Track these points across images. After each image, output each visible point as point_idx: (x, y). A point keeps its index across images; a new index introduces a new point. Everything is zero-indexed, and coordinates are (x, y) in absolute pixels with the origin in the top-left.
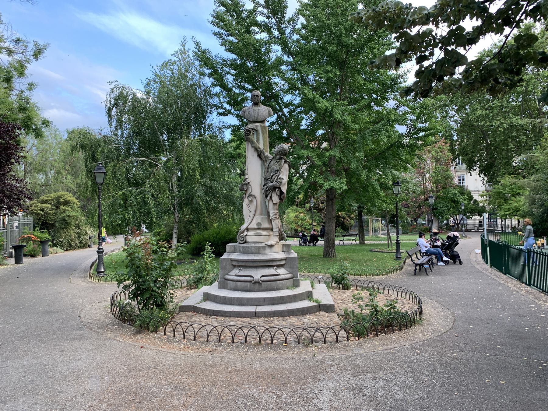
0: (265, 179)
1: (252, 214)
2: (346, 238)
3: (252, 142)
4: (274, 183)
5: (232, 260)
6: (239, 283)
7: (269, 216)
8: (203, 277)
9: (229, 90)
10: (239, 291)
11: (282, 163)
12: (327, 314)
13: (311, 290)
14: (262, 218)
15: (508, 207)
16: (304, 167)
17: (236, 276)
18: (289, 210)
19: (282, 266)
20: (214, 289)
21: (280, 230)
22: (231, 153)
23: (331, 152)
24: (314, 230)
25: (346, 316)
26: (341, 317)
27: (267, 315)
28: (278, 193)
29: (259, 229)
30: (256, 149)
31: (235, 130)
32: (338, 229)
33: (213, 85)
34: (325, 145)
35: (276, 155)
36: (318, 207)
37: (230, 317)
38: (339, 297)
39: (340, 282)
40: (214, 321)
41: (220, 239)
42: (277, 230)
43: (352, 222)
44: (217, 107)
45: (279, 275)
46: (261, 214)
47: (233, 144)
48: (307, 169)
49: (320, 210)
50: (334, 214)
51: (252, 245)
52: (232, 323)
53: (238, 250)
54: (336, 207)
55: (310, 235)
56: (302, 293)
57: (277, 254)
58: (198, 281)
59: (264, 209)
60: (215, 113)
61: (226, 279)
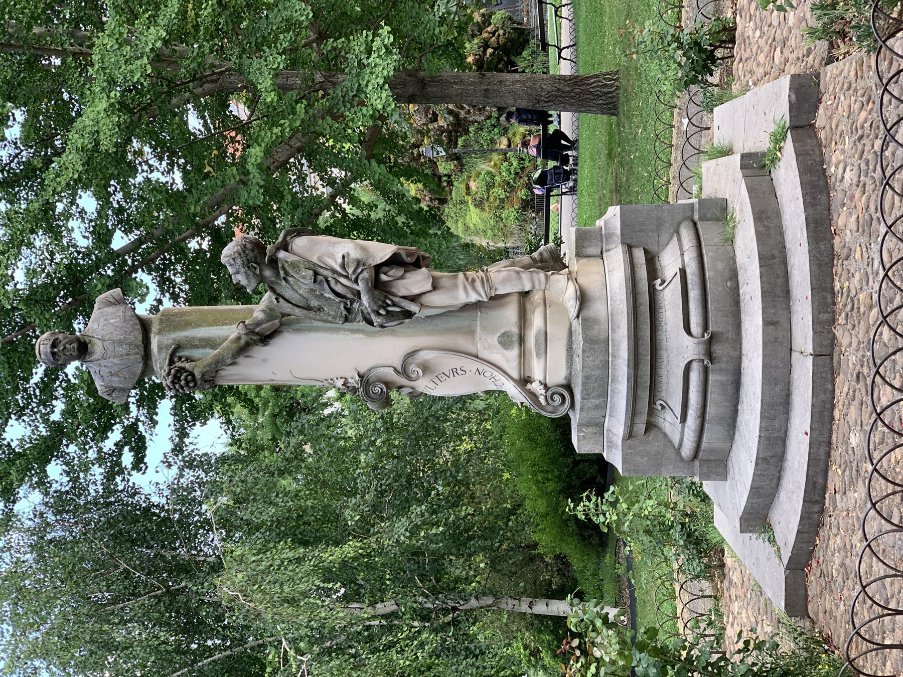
0: (346, 320)
1: (471, 365)
2: (551, 39)
3: (218, 365)
4: (361, 287)
5: (630, 435)
6: (711, 410)
7: (478, 305)
8: (683, 525)
9: (58, 432)
10: (735, 412)
11: (291, 258)
12: (827, 101)
13: (736, 159)
14: (484, 328)
16: (313, 179)
17: (684, 419)
18: (457, 229)
19: (651, 260)
20: (728, 501)
21: (526, 267)
22: (274, 416)
23: (265, 83)
24: (525, 144)
25: (834, 33)
26: (835, 52)
27: (826, 317)
28: (396, 272)
29: (522, 340)
30: (243, 349)
31: (189, 414)
32: (521, 65)
33: (43, 484)
34: (239, 109)
35: (261, 279)
36: (450, 132)
37: (829, 443)
38: (761, 58)
39: (708, 57)
40: (847, 500)
41: (553, 461)
42: (525, 276)
43: (498, 16)
44: (114, 470)
45: (683, 272)
46: (471, 332)
47: (239, 411)
48: (320, 169)
49: (459, 126)
50: (471, 76)
52: (855, 440)
53: (596, 414)
54: (448, 71)
55: (539, 160)
56: (750, 190)
57: (611, 276)
58: (697, 543)
59: (453, 322)
60: (136, 478)
61: (695, 456)
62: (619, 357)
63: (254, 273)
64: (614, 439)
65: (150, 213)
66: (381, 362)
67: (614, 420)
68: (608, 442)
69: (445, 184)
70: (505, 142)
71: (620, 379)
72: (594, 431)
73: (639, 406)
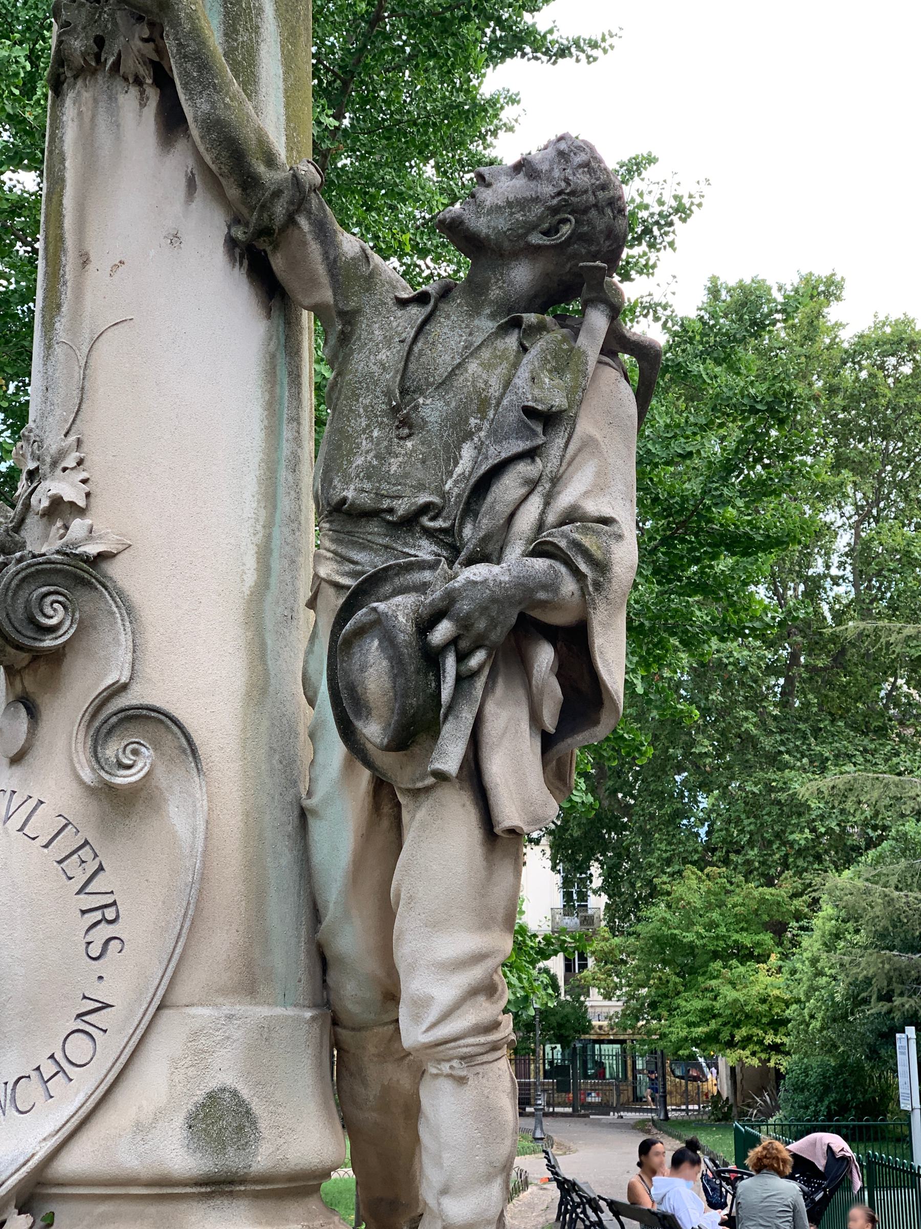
14: (265, 1033)
15: (698, 1004)
46: (249, 983)
63: (531, 227)
65: (411, 57)
66: (153, 638)
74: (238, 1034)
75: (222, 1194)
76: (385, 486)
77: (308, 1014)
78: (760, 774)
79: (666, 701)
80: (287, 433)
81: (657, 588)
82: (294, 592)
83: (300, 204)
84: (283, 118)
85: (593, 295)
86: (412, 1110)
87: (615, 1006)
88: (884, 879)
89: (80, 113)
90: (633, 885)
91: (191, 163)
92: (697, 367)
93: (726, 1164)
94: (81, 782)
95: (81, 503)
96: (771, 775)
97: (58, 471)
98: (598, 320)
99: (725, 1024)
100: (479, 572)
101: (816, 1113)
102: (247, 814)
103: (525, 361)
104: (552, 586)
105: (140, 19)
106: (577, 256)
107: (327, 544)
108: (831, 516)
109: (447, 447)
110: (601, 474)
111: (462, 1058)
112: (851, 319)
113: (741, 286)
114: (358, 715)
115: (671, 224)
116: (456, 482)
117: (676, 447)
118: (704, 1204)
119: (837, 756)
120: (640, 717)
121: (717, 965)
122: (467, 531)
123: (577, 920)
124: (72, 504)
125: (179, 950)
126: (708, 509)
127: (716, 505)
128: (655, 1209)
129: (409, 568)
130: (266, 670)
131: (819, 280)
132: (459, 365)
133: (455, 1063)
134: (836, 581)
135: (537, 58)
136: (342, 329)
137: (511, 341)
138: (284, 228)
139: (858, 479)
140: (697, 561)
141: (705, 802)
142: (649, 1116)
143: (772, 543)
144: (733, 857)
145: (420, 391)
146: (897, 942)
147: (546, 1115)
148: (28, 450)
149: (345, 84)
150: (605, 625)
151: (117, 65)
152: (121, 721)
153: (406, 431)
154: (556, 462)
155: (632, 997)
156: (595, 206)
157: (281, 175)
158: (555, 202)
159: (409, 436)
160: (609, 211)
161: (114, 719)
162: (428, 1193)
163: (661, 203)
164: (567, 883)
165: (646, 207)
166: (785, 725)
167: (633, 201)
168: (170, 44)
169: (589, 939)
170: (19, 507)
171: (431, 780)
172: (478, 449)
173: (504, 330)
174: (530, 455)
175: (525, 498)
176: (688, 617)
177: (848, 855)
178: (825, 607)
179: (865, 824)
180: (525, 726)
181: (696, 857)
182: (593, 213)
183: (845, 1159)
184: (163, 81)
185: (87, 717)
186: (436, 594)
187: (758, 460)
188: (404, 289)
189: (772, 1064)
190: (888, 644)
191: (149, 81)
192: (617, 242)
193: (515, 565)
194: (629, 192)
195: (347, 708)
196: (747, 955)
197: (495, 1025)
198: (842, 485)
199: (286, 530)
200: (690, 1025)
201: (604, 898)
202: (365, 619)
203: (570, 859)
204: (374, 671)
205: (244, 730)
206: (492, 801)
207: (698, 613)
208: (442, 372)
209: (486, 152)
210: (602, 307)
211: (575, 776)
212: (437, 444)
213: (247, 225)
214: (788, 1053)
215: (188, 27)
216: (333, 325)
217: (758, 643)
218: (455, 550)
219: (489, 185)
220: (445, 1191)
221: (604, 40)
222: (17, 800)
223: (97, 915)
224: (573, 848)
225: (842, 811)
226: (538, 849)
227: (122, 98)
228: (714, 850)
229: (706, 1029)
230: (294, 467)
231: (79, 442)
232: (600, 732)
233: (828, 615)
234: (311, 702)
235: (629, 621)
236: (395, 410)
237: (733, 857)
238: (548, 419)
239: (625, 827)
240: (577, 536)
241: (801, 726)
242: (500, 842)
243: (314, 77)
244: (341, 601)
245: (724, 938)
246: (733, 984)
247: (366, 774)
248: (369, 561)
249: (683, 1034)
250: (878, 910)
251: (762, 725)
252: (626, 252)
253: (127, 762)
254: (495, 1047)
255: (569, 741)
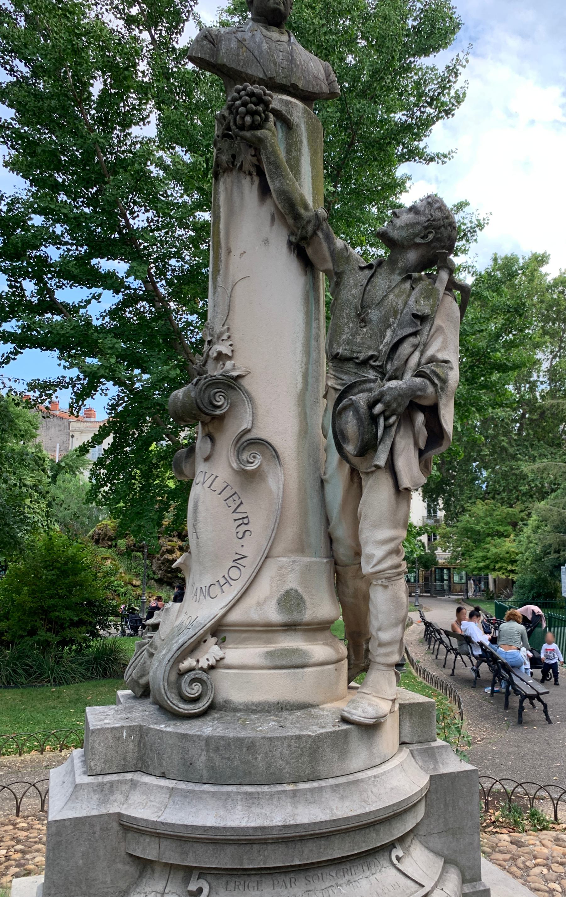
5: (129, 827)
14: (308, 568)
15: (481, 554)
29: (290, 627)
46: (301, 548)
51: (267, 727)
62: (295, 805)
63: (416, 235)
64: (119, 797)
66: (261, 411)
67: (164, 797)
68: (112, 783)
69: (110, 543)
70: (138, 583)
71: (256, 810)
72: (130, 756)
73: (200, 849)
74: (297, 568)
75: (292, 630)
76: (355, 347)
77: (325, 560)
78: (508, 463)
79: (470, 433)
80: (314, 325)
81: (467, 387)
82: (318, 392)
83: (318, 226)
84: (311, 189)
85: (442, 264)
86: (366, 598)
87: (448, 554)
88: (558, 505)
89: (226, 188)
90: (455, 507)
91: (273, 209)
92: (485, 293)
93: (492, 617)
94: (233, 469)
95: (230, 354)
96: (512, 463)
97: (220, 341)
98: (444, 276)
99: (492, 562)
100: (394, 383)
101: (528, 597)
102: (300, 482)
103: (413, 294)
104: (423, 389)
105: (250, 147)
106: (434, 248)
107: (331, 372)
108: (539, 355)
109: (380, 331)
110: (444, 342)
111: (386, 578)
112: (551, 272)
113: (506, 258)
114: (344, 442)
115: (475, 232)
116: (384, 346)
117: (476, 327)
118: (482, 632)
119: (540, 456)
120: (459, 440)
121: (489, 539)
122: (389, 367)
123: (433, 521)
124: (226, 355)
125: (273, 535)
126: (489, 353)
127: (492, 351)
128: (463, 634)
129: (365, 382)
130: (307, 424)
131: (539, 256)
132: (386, 296)
133: (383, 580)
134: (542, 383)
135: (420, 162)
136: (337, 280)
137: (407, 285)
138: (312, 237)
139: (552, 340)
140: (483, 375)
141: (485, 474)
142: (460, 597)
143: (516, 367)
144: (496, 496)
145: (369, 307)
146: (562, 530)
147: (420, 596)
148: (207, 332)
149: (338, 172)
150: (445, 406)
151: (241, 167)
152: (248, 444)
153: (364, 324)
154: (426, 337)
155: (455, 551)
156: (444, 226)
157: (310, 214)
158: (426, 224)
159: (365, 326)
160: (449, 228)
161: (245, 444)
162: (373, 630)
163: (471, 222)
164: (429, 506)
165: (465, 224)
166: (520, 442)
167: (459, 221)
168: (263, 158)
169: (437, 528)
170: (205, 356)
171: (374, 469)
172: (394, 331)
173: (404, 280)
174: (415, 334)
175: (413, 353)
176: (480, 399)
177: (543, 495)
178: (538, 394)
179: (551, 483)
180: (412, 447)
181: (481, 496)
182: (443, 229)
183: (540, 616)
184: (261, 173)
185: (235, 442)
186: (376, 393)
187: (511, 332)
188: (363, 262)
189: (510, 578)
190: (563, 409)
191: (255, 174)
192: (452, 241)
193: (408, 380)
194: (457, 218)
195: (340, 439)
196: (501, 535)
197: (399, 566)
198: (545, 342)
199: (314, 366)
200: (478, 562)
201: (444, 512)
202: (347, 403)
203: (431, 497)
204: (350, 424)
205: (298, 448)
206: (399, 477)
207: (484, 397)
208: (378, 299)
209: (397, 201)
210: (446, 270)
211: (432, 464)
212: (376, 330)
213: (296, 236)
214: (517, 573)
215: (271, 150)
216: (332, 278)
217: (509, 409)
218: (384, 375)
219: (398, 217)
220: (379, 629)
221: (449, 154)
222: (207, 475)
223: (241, 522)
224: (431, 493)
225: (542, 478)
226: (417, 493)
227: (243, 181)
228: (489, 493)
229: (484, 564)
230: (317, 339)
231: (228, 329)
232: (443, 449)
233: (539, 397)
234: (325, 437)
235: (455, 401)
236: (359, 315)
237: (496, 496)
238: (422, 319)
239: (452, 484)
240: (434, 368)
241: (526, 443)
242: (402, 493)
243: (324, 169)
244: (337, 396)
245: (492, 528)
246: (495, 546)
247: (347, 466)
248: (348, 379)
249: (475, 566)
250: (555, 517)
251: (510, 443)
252: (457, 244)
253: (251, 461)
254: (399, 574)
255: (430, 452)
